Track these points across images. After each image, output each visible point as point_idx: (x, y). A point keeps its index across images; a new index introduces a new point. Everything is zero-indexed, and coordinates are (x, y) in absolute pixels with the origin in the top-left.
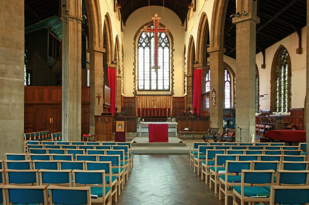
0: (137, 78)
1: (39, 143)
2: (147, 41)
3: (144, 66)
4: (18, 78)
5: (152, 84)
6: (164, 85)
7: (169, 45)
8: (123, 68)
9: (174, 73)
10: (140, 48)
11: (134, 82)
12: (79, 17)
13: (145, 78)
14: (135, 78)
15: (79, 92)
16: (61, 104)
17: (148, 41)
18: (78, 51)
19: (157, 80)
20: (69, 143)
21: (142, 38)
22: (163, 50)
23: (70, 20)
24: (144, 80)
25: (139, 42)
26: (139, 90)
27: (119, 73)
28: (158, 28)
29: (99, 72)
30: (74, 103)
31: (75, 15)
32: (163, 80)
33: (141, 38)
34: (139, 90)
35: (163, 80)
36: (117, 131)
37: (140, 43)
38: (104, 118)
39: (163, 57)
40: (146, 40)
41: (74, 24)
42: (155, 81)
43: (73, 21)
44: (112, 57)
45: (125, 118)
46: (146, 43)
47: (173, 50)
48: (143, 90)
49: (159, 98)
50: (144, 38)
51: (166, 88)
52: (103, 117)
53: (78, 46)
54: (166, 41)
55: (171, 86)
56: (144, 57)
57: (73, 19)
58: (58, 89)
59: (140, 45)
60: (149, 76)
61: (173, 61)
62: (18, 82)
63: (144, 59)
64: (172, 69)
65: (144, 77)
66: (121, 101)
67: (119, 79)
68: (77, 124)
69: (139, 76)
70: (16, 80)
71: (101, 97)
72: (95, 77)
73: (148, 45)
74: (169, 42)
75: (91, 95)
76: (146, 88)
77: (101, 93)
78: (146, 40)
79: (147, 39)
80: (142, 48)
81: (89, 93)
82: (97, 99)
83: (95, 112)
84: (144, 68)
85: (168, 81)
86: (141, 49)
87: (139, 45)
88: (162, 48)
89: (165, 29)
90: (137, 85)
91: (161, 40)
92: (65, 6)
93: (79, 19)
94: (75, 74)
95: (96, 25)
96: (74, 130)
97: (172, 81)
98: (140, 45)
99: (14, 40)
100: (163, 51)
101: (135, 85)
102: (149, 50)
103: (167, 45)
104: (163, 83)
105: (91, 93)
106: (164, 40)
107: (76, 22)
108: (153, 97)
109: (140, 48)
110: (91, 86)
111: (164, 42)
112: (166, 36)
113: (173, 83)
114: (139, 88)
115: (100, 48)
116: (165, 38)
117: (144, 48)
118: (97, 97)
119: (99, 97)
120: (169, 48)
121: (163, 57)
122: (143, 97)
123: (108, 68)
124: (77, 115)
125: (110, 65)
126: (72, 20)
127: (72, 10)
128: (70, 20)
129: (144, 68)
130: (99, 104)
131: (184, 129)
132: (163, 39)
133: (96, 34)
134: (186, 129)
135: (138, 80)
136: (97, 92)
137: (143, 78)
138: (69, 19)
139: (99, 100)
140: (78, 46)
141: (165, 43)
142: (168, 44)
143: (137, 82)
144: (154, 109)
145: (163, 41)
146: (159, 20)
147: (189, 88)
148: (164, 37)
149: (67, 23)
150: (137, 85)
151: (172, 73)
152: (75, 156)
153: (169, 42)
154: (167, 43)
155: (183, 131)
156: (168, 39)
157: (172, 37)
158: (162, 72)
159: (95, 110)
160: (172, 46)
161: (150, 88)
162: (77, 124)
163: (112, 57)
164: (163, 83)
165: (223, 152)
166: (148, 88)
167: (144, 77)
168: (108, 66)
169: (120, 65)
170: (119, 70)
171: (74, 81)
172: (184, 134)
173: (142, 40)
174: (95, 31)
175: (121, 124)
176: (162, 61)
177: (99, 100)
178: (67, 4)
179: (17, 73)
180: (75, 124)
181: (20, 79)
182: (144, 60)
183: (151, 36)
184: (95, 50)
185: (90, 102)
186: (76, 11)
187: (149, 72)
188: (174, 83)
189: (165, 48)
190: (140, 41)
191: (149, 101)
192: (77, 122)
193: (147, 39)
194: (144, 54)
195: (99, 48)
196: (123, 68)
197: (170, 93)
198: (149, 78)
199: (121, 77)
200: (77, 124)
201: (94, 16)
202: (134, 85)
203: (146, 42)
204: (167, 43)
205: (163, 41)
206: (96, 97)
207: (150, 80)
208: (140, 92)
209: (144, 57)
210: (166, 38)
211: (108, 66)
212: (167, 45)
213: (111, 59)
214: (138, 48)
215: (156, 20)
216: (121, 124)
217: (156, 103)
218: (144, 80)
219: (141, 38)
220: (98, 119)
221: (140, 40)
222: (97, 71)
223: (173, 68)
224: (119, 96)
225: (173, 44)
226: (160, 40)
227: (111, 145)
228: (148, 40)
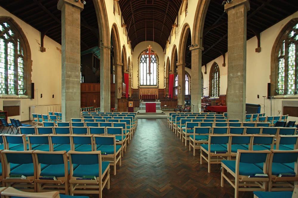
0: (139, 79)
5: (147, 82)
14: (138, 79)
25: (140, 60)
26: (141, 85)
41: (106, 50)
47: (158, 64)
49: (151, 89)
51: (155, 84)
55: (157, 83)
57: (106, 48)
61: (158, 70)
62: (77, 81)
74: (156, 60)
82: (119, 90)
90: (139, 83)
97: (158, 80)
101: (138, 83)
112: (155, 57)
113: (158, 81)
119: (120, 89)
120: (156, 63)
130: (120, 93)
134: (165, 106)
143: (139, 81)
145: (143, 60)
150: (139, 83)
151: (158, 76)
153: (156, 60)
156: (156, 59)
157: (158, 58)
160: (158, 62)
161: (147, 84)
186: (108, 43)
193: (145, 58)
205: (153, 60)
206: (118, 89)
213: (126, 69)
214: (140, 63)
225: (158, 61)
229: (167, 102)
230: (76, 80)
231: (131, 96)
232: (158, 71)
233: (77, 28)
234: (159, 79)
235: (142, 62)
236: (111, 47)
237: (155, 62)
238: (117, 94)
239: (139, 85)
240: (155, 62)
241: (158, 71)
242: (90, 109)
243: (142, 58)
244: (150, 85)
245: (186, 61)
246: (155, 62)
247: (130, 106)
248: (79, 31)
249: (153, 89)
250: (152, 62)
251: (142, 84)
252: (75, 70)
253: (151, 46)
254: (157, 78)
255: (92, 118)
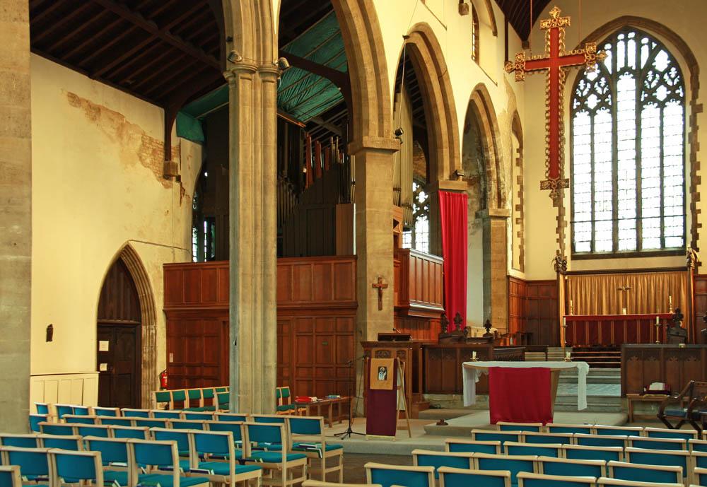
0: (567, 218)
1: (118, 413)
2: (603, 88)
3: (593, 173)
4: (16, 255)
5: (621, 235)
6: (666, 234)
7: (684, 91)
8: (522, 187)
9: (699, 188)
10: (577, 114)
11: (559, 229)
12: (268, 64)
13: (596, 214)
15: (271, 275)
16: (228, 311)
17: (606, 89)
18: (265, 161)
19: (639, 218)
20: (213, 417)
21: (586, 81)
22: (662, 113)
23: (243, 76)
24: (593, 222)
25: (574, 96)
26: (575, 257)
27: (499, 206)
28: (560, 55)
29: (381, 210)
30: (256, 308)
31: (258, 60)
32: (662, 217)
33: (582, 82)
34: (575, 257)
35: (662, 217)
36: (371, 388)
37: (647, 91)
38: (387, 349)
39: (662, 137)
40: (599, 85)
41: (254, 86)
42: (633, 223)
43: (250, 80)
44: (452, 156)
45: (458, 351)
46: (599, 96)
47: (697, 109)
48: (591, 256)
49: (643, 281)
50: (662, 70)
51: (674, 243)
52: (383, 345)
53: (265, 146)
54: (673, 80)
55: (690, 237)
56: (592, 145)
57: (253, 72)
58: (313, 266)
59: (579, 103)
60: (610, 208)
61: (695, 147)
62: (17, 262)
63: (592, 149)
64: (693, 175)
65: (593, 213)
66: (508, 296)
67: (500, 224)
68: (265, 368)
69: (576, 210)
70: (11, 258)
71: (386, 286)
72: (368, 225)
73: (609, 102)
74: (681, 83)
75: (358, 282)
76: (599, 249)
77: (385, 274)
78: (599, 85)
79: (603, 80)
80: (587, 113)
81: (354, 275)
82: (375, 292)
83: (368, 331)
84: (593, 182)
85: (681, 219)
86: (582, 118)
87: (576, 104)
88: (656, 105)
89: (583, 55)
90: (567, 241)
91: (654, 78)
92: (230, 40)
93: (268, 69)
94: (256, 226)
95: (369, 69)
96: (256, 383)
97: (695, 219)
98: (579, 103)
99: (5, 163)
100: (662, 117)
101: (560, 241)
102: (610, 119)
103: (677, 91)
104: (662, 228)
105: (358, 276)
106: (666, 77)
107: (259, 79)
108: (621, 278)
109: (577, 114)
110: (359, 256)
111: (666, 84)
112: (673, 63)
113: (696, 225)
114: (577, 250)
115: (382, 138)
116: (668, 71)
117: (592, 113)
118: (374, 286)
119: (380, 288)
120: (683, 102)
121: (662, 137)
122: (588, 278)
123: (440, 192)
124: (265, 342)
125: (445, 183)
126: (248, 76)
127: (246, 50)
128: (242, 78)
129: (593, 182)
130: (380, 308)
131: (647, 387)
132: (662, 74)
133: (369, 97)
134: (657, 386)
135: (572, 223)
136: (374, 270)
137: (590, 215)
138: (240, 75)
139: (380, 295)
140: (265, 146)
141: (669, 88)
142: (680, 91)
143: (567, 231)
144: (619, 320)
145: (593, 91)
146: (563, 26)
147: (501, 256)
148: (666, 66)
149: (236, 84)
150: (567, 241)
151: (693, 189)
152: (517, 479)
153: (681, 83)
154: (676, 87)
155: (644, 393)
156: (679, 73)
157: (693, 64)
158: (658, 190)
159: (368, 327)
160: (695, 96)
161: (615, 246)
162: (265, 367)
163: (452, 156)
164: (662, 228)
165: (493, 449)
166: (608, 248)
167: (593, 213)
168: (440, 187)
169: (502, 179)
170: (499, 194)
171: (256, 245)
172: (652, 403)
173: (585, 87)
174: (366, 88)
175: (385, 368)
176: (659, 151)
177: (380, 295)
178: (235, 35)
179: (13, 242)
180: (259, 365)
181: (21, 255)
182: (592, 155)
183: (618, 70)
184: (365, 145)
185: (356, 302)
186: (261, 50)
187: (611, 194)
188: (700, 226)
189: (598, 111)
190: (579, 93)
191: (608, 291)
192: (265, 360)
193: (603, 81)
194: (592, 134)
195: (379, 138)
196: (522, 187)
197: (681, 261)
198: (609, 215)
199: (506, 218)
200: (265, 368)
201: (358, 45)
202: (558, 240)
203: (600, 91)
204: (676, 87)
205: (662, 82)
206: (369, 286)
207: (615, 220)
208: (579, 262)
209: (592, 145)
210: (673, 70)
211: (440, 187)
212: (677, 91)
213: (452, 163)
214: (573, 115)
215: (552, 29)
216: (385, 368)
217: (634, 296)
218: (593, 222)
219: (582, 82)
220: (370, 352)
221: (579, 87)
222: (374, 209)
223: (698, 173)
224: (499, 280)
225: (695, 87)
226: (650, 79)
227: (499, 442)
228: (606, 84)
229: (672, 363)
230: (13, 258)
231: (504, 326)
232: (693, 156)
233: (16, 19)
234: (698, 205)
235: (583, 107)
236: (281, 63)
237: (672, 96)
238: (364, 317)
239: (568, 253)
240: (672, 96)
241: (693, 156)
242: (281, 401)
243: (582, 83)
244: (638, 253)
245: (337, 125)
246: (676, 97)
247: (101, 370)
248: (23, 37)
249: (653, 276)
250: (654, 100)
251: (583, 248)
252: (7, 212)
253: (563, 15)
254: (689, 201)
255: (71, 434)
